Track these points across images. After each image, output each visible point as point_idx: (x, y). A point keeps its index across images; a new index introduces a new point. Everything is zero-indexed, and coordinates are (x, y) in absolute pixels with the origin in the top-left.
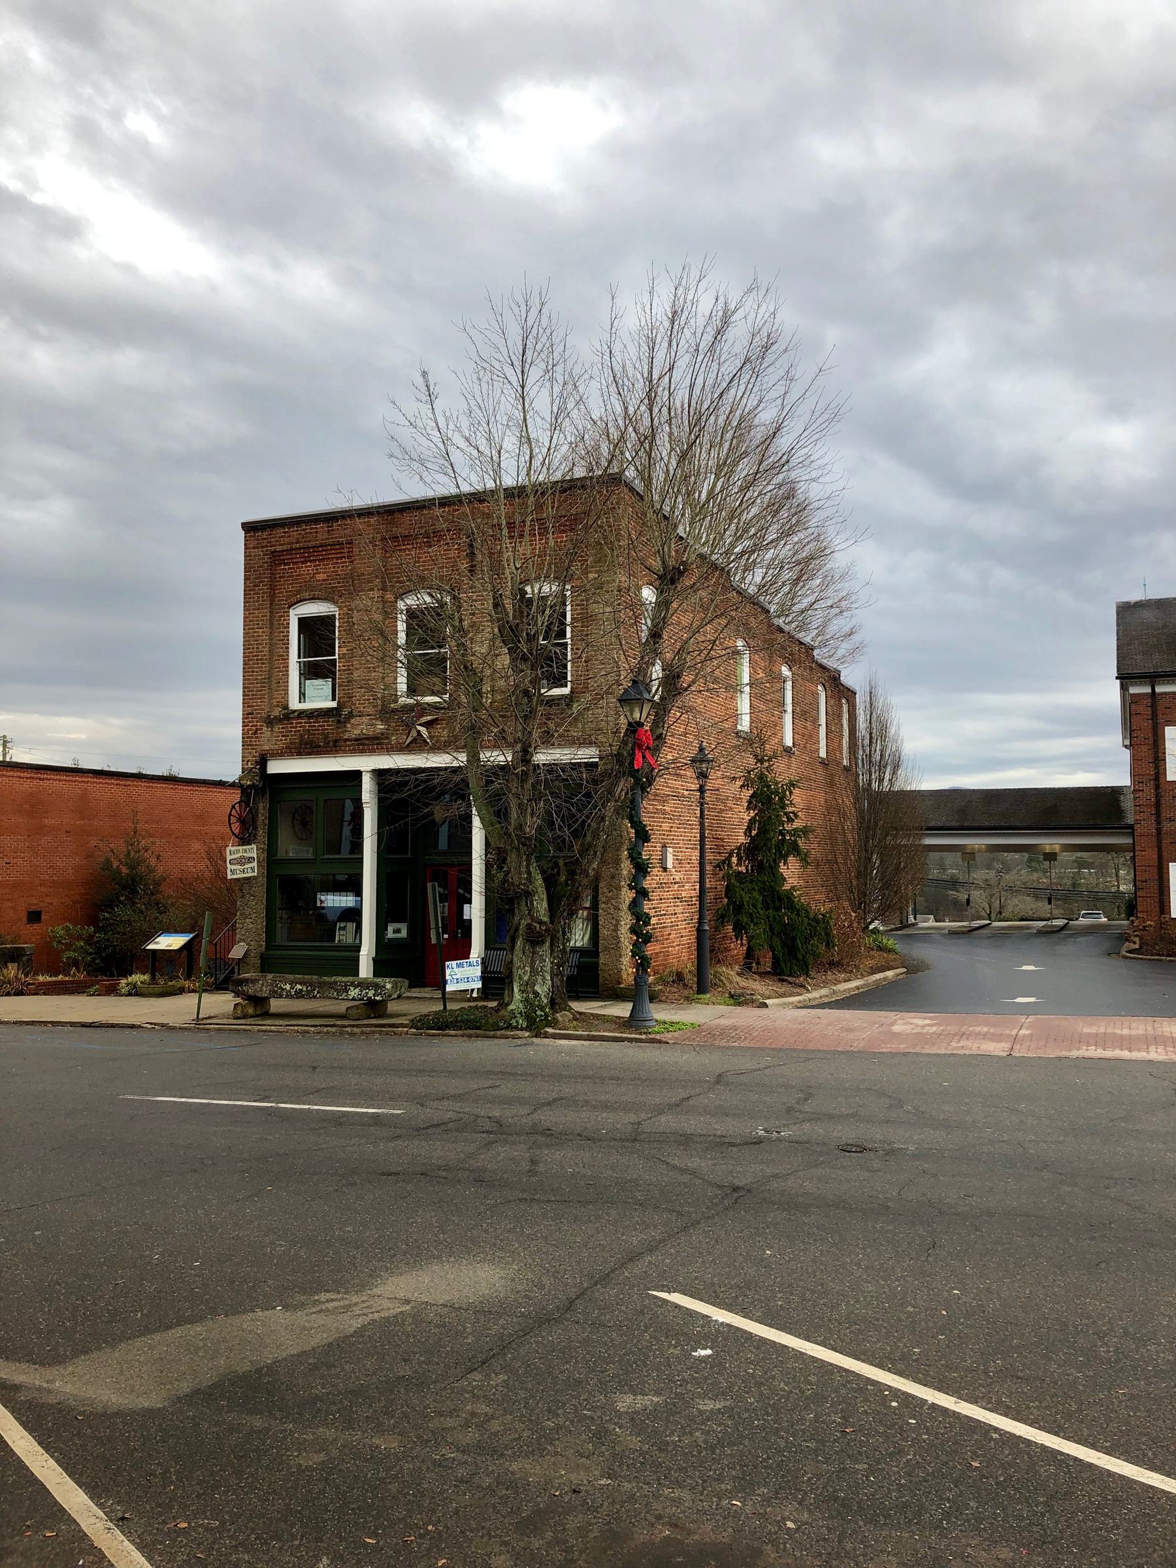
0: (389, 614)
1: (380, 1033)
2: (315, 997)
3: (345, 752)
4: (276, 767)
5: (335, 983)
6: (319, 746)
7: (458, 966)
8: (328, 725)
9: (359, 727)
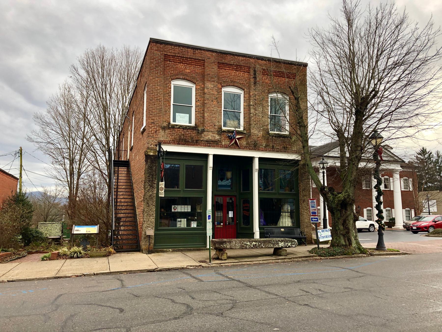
0: (264, 99)
1: (407, 251)
2: (262, 247)
3: (201, 145)
4: (166, 148)
5: (271, 241)
6: (189, 142)
7: (322, 231)
8: (193, 134)
9: (209, 136)
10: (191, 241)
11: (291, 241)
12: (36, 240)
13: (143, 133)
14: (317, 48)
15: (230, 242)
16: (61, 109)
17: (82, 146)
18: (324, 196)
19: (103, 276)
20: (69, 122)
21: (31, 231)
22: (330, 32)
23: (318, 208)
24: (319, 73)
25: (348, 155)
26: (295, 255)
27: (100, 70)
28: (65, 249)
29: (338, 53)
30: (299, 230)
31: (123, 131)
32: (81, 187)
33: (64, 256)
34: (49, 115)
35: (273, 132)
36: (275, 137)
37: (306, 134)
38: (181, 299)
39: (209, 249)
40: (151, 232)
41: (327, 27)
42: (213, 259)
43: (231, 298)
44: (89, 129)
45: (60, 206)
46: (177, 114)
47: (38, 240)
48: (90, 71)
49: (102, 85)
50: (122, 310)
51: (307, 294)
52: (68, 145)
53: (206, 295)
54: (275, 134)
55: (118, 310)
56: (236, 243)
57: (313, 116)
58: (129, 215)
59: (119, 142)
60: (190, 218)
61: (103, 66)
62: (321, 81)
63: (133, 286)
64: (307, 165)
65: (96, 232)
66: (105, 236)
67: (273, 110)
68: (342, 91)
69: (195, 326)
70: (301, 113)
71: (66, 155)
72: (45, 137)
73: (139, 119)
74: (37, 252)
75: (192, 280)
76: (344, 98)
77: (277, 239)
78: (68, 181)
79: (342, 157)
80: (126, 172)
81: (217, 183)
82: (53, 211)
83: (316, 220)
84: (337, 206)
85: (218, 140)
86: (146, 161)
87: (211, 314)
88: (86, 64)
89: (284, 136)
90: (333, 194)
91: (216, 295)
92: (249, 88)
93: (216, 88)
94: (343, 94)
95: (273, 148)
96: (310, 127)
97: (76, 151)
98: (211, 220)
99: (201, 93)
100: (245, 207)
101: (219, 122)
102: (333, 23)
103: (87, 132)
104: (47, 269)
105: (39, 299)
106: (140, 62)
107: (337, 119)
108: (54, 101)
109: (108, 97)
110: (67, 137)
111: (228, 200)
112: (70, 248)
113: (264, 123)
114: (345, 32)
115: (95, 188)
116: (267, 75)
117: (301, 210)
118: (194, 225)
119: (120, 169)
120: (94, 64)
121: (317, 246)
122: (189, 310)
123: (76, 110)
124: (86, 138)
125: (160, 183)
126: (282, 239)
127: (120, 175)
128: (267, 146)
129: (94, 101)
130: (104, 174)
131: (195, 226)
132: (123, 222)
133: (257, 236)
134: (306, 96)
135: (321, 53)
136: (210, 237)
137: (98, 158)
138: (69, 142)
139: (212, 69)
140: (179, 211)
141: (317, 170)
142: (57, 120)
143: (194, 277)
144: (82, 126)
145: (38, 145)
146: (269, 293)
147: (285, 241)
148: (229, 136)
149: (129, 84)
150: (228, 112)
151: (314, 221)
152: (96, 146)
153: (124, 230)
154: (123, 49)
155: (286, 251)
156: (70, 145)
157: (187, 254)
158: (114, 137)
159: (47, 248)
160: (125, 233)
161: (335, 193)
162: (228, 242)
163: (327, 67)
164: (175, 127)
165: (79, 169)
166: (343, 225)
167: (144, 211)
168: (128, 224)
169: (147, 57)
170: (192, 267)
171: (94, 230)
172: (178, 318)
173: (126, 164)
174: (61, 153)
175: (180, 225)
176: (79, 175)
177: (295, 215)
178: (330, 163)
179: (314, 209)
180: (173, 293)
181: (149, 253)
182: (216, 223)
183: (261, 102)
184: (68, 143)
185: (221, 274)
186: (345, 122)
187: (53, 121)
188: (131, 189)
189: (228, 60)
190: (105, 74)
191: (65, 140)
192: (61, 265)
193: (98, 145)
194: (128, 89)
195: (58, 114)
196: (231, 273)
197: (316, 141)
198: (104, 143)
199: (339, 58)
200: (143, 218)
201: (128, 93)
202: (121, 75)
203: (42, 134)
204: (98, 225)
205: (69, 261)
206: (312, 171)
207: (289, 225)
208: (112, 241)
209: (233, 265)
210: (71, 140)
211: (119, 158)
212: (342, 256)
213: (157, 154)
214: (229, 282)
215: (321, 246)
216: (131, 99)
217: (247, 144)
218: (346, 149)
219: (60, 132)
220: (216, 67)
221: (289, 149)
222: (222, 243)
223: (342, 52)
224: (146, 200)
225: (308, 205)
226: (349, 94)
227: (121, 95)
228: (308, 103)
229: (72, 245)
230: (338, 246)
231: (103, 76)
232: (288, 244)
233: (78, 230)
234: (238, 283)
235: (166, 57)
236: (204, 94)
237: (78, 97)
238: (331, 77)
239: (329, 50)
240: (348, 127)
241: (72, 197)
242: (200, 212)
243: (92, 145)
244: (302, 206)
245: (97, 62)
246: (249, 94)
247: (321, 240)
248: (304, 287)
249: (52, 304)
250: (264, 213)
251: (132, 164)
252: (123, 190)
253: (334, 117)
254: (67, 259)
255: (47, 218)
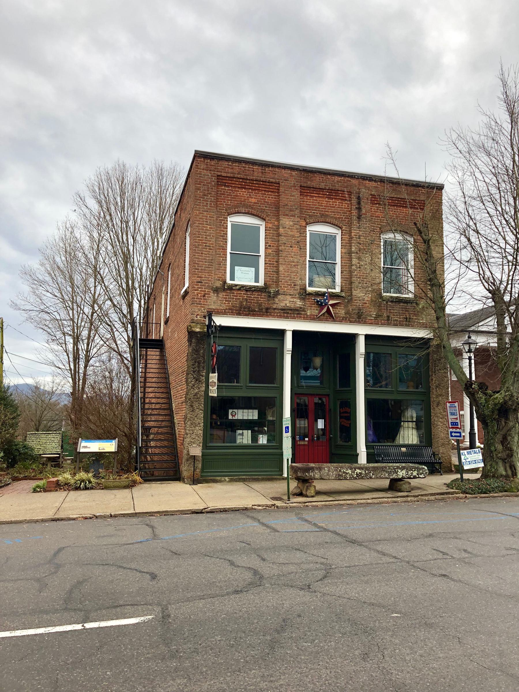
2: (371, 478)
3: (274, 316)
4: (220, 321)
5: (386, 467)
6: (255, 311)
7: (468, 453)
8: (262, 299)
10: (260, 466)
11: (418, 468)
12: (25, 459)
13: (184, 297)
14: (459, 159)
15: (320, 469)
16: (60, 260)
17: (92, 315)
18: (472, 396)
19: (124, 519)
20: (71, 279)
21: (16, 445)
22: (482, 133)
23: (461, 413)
24: (463, 199)
25: (509, 330)
26: (425, 490)
27: (119, 200)
28: (67, 476)
29: (494, 167)
30: (430, 451)
31: (154, 293)
32: (90, 380)
33: (66, 486)
34: (43, 269)
35: (388, 294)
36: (392, 302)
37: (442, 297)
38: (243, 560)
39: (287, 479)
40: (196, 451)
41: (475, 126)
42: (294, 495)
43: (323, 560)
44: (102, 290)
45: (58, 407)
46: (236, 268)
47: (27, 459)
48: (103, 202)
49: (121, 222)
50: (154, 576)
51: (445, 556)
52: (71, 315)
53: (283, 554)
54: (391, 297)
55: (148, 576)
56: (329, 471)
57: (453, 268)
58: (164, 424)
59: (148, 311)
60: (256, 429)
61: (123, 194)
62: (466, 213)
63: (171, 537)
64: (444, 347)
65: (114, 451)
66: (126, 455)
67: (389, 259)
68: (500, 229)
69: (267, 607)
70: (433, 264)
71: (67, 330)
72: (37, 303)
73: (179, 275)
74: (26, 478)
75: (261, 529)
76: (504, 239)
77: (394, 464)
78: (71, 370)
79: (500, 333)
80: (158, 357)
81: (298, 373)
82: (48, 415)
83: (458, 434)
84: (493, 412)
85: (301, 308)
86: (190, 341)
87: (292, 587)
88: (97, 191)
89: (406, 301)
90: (486, 394)
91: (298, 554)
92: (350, 225)
93: (298, 227)
94: (502, 234)
95: (388, 320)
96: (448, 288)
97: (83, 324)
98: (289, 434)
99: (274, 235)
100: (343, 413)
101: (303, 279)
102: (486, 119)
103: (99, 294)
104: (41, 506)
105: (31, 554)
106: (179, 186)
107: (492, 274)
108: (49, 247)
109: (131, 240)
110: (70, 303)
111: (316, 400)
112: (75, 474)
113: (373, 279)
114: (506, 133)
115: (112, 380)
116: (379, 204)
117: (434, 419)
118: (263, 440)
119: (149, 353)
120: (110, 190)
121: (459, 476)
122: (258, 580)
123: (83, 260)
124: (98, 304)
125: (211, 375)
126: (404, 465)
127: (149, 362)
128: (378, 316)
129: (110, 247)
130: (126, 359)
131: (265, 442)
132: (155, 434)
133: (363, 459)
134: (441, 237)
135: (466, 168)
136: (288, 460)
137: (117, 334)
138: (73, 309)
139: (291, 196)
140: (240, 417)
141: (458, 353)
142: (53, 276)
143: (263, 524)
144: (92, 285)
145: (26, 315)
146: (384, 554)
147: (408, 469)
148: (318, 302)
149: (162, 221)
150: (316, 264)
151: (455, 436)
152: (113, 316)
153: (156, 447)
154: (154, 165)
155: (410, 483)
156: (73, 315)
157: (253, 486)
158: (140, 302)
159: (41, 473)
160: (157, 451)
161: (489, 392)
162: (317, 468)
163: (475, 191)
164: (234, 288)
165: (88, 351)
166: (502, 443)
167: (186, 418)
168: (162, 437)
169: (190, 180)
170: (260, 508)
171: (110, 446)
172: (241, 591)
173: (159, 344)
174: (61, 327)
175: (241, 441)
176: (87, 360)
177: (424, 425)
178: (481, 341)
179: (455, 417)
180: (231, 551)
181: (194, 484)
182: (297, 438)
183: (368, 247)
184: (71, 312)
185: (306, 521)
186: (505, 278)
187: (48, 279)
188: (167, 383)
189: (317, 181)
190: (126, 205)
191: (66, 307)
192: (61, 500)
193: (115, 314)
194: (161, 228)
195: (56, 268)
196: (322, 518)
197: (457, 306)
198: (125, 312)
199: (495, 175)
200: (185, 429)
201: (162, 234)
202: (149, 207)
203: (32, 298)
204: (117, 439)
205: (73, 494)
206: (451, 356)
207: (415, 442)
208: (137, 463)
209: (326, 505)
210: (75, 307)
211: (147, 335)
212: (501, 494)
213: (206, 330)
214: (320, 534)
215: (466, 476)
216: (167, 243)
217: (346, 314)
218: (507, 320)
219: (58, 295)
220: (296, 194)
221: (415, 322)
222: (308, 470)
223: (500, 166)
224: (190, 402)
225: (445, 409)
226: (512, 231)
227: (150, 238)
228: (445, 247)
229: (77, 468)
230: (493, 476)
231: (123, 208)
232: (412, 473)
233: (85, 447)
234: (335, 536)
235: (221, 180)
236: (279, 235)
237: (86, 242)
238: (483, 207)
239: (479, 162)
240: (510, 286)
241: (76, 394)
242: (273, 421)
243: (107, 315)
244: (436, 411)
245: (114, 186)
246: (350, 235)
247: (466, 467)
248: (438, 544)
249: (50, 562)
250: (373, 423)
251: (168, 344)
252: (154, 385)
253: (486, 270)
254: (70, 490)
255: (39, 425)
